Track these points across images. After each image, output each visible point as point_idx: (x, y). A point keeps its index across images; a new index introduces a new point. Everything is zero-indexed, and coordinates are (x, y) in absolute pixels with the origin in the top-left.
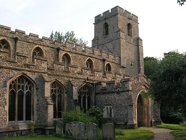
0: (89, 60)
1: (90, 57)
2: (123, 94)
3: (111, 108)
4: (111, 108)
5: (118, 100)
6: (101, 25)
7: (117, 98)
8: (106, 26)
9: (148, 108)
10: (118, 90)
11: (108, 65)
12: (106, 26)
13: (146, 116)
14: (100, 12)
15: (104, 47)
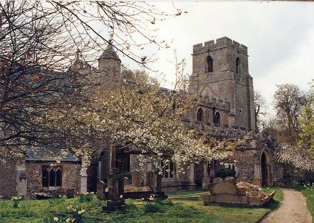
0: (200, 109)
1: (201, 106)
2: (248, 151)
3: (233, 166)
4: (233, 166)
5: (242, 157)
6: (203, 59)
7: (241, 156)
8: (210, 60)
9: (270, 167)
10: (243, 148)
11: (218, 113)
12: (210, 60)
13: (269, 176)
14: (202, 40)
15: (206, 88)
